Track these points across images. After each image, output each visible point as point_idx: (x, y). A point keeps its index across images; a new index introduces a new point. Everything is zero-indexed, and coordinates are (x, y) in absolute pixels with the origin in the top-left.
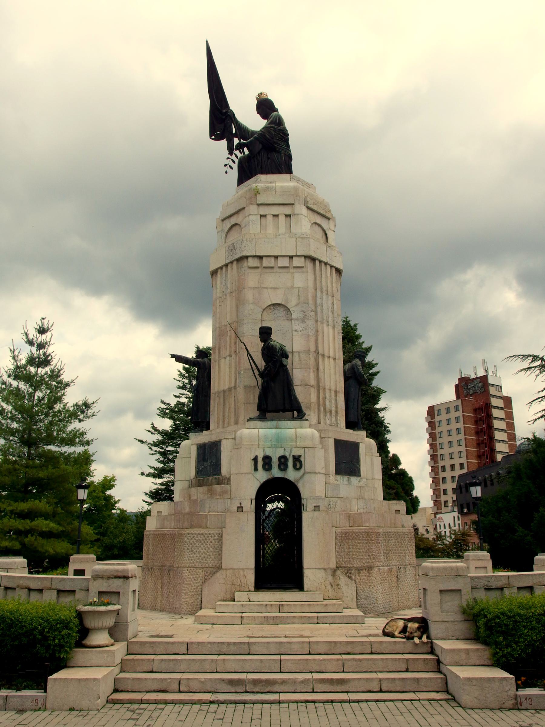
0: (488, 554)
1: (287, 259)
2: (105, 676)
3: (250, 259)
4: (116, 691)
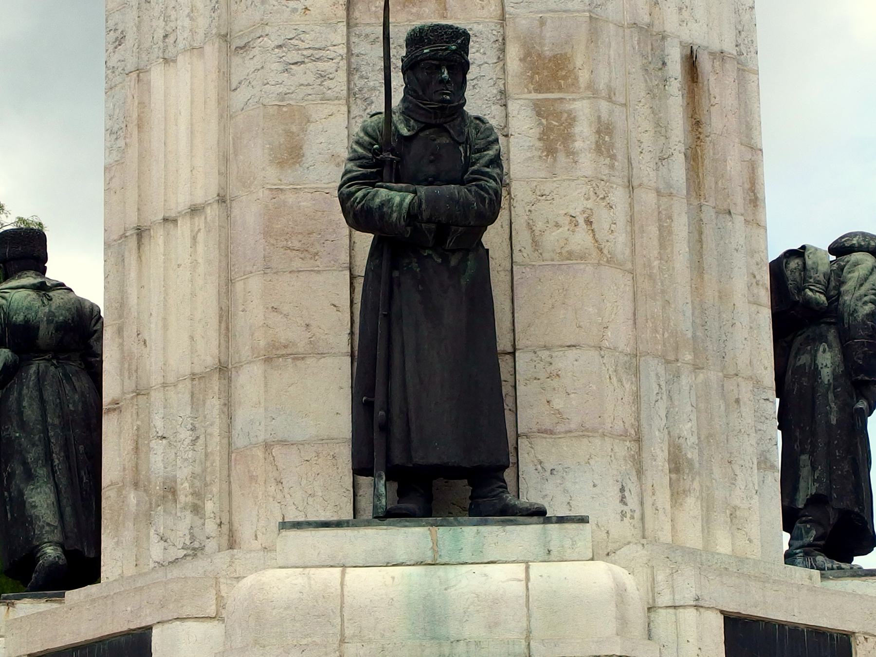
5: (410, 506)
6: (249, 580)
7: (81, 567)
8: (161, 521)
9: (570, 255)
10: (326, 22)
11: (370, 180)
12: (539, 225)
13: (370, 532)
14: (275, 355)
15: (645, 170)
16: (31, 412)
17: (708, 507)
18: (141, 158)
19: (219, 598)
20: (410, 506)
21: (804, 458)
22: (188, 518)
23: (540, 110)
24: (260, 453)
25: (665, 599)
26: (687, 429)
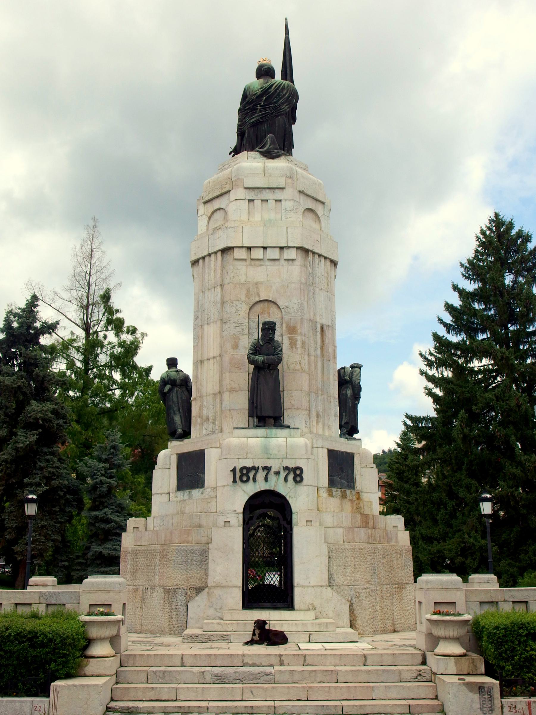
0: (496, 577)
1: (278, 250)
2: (104, 684)
3: (236, 250)
4: (112, 700)
5: (261, 424)
6: (227, 440)
7: (186, 434)
8: (206, 425)
9: (296, 370)
10: (244, 318)
11: (254, 354)
12: (289, 364)
13: (253, 430)
14: (232, 390)
15: (312, 352)
16: (175, 399)
17: (324, 425)
18: (202, 345)
19: (220, 443)
20: (261, 424)
21: (344, 414)
22: (212, 425)
23: (290, 338)
24: (228, 411)
25: (315, 446)
26: (320, 408)
